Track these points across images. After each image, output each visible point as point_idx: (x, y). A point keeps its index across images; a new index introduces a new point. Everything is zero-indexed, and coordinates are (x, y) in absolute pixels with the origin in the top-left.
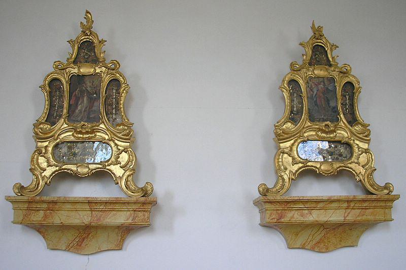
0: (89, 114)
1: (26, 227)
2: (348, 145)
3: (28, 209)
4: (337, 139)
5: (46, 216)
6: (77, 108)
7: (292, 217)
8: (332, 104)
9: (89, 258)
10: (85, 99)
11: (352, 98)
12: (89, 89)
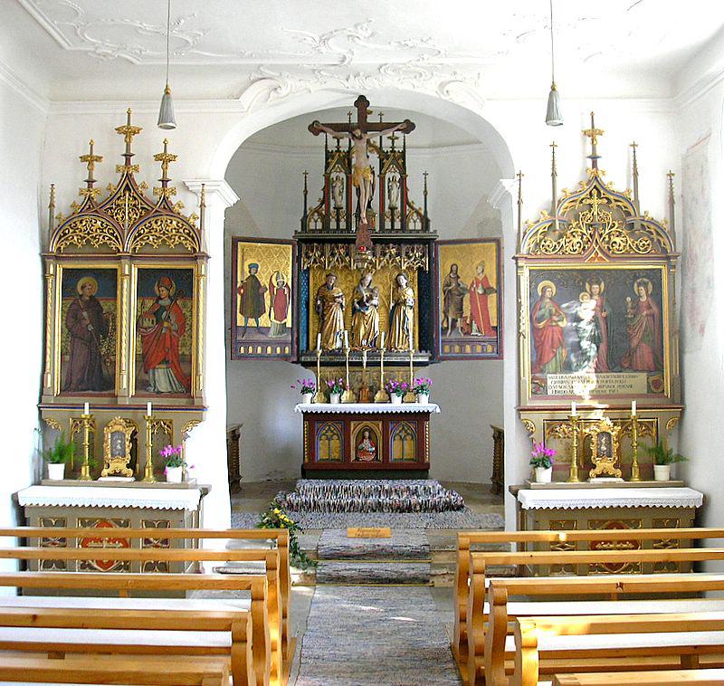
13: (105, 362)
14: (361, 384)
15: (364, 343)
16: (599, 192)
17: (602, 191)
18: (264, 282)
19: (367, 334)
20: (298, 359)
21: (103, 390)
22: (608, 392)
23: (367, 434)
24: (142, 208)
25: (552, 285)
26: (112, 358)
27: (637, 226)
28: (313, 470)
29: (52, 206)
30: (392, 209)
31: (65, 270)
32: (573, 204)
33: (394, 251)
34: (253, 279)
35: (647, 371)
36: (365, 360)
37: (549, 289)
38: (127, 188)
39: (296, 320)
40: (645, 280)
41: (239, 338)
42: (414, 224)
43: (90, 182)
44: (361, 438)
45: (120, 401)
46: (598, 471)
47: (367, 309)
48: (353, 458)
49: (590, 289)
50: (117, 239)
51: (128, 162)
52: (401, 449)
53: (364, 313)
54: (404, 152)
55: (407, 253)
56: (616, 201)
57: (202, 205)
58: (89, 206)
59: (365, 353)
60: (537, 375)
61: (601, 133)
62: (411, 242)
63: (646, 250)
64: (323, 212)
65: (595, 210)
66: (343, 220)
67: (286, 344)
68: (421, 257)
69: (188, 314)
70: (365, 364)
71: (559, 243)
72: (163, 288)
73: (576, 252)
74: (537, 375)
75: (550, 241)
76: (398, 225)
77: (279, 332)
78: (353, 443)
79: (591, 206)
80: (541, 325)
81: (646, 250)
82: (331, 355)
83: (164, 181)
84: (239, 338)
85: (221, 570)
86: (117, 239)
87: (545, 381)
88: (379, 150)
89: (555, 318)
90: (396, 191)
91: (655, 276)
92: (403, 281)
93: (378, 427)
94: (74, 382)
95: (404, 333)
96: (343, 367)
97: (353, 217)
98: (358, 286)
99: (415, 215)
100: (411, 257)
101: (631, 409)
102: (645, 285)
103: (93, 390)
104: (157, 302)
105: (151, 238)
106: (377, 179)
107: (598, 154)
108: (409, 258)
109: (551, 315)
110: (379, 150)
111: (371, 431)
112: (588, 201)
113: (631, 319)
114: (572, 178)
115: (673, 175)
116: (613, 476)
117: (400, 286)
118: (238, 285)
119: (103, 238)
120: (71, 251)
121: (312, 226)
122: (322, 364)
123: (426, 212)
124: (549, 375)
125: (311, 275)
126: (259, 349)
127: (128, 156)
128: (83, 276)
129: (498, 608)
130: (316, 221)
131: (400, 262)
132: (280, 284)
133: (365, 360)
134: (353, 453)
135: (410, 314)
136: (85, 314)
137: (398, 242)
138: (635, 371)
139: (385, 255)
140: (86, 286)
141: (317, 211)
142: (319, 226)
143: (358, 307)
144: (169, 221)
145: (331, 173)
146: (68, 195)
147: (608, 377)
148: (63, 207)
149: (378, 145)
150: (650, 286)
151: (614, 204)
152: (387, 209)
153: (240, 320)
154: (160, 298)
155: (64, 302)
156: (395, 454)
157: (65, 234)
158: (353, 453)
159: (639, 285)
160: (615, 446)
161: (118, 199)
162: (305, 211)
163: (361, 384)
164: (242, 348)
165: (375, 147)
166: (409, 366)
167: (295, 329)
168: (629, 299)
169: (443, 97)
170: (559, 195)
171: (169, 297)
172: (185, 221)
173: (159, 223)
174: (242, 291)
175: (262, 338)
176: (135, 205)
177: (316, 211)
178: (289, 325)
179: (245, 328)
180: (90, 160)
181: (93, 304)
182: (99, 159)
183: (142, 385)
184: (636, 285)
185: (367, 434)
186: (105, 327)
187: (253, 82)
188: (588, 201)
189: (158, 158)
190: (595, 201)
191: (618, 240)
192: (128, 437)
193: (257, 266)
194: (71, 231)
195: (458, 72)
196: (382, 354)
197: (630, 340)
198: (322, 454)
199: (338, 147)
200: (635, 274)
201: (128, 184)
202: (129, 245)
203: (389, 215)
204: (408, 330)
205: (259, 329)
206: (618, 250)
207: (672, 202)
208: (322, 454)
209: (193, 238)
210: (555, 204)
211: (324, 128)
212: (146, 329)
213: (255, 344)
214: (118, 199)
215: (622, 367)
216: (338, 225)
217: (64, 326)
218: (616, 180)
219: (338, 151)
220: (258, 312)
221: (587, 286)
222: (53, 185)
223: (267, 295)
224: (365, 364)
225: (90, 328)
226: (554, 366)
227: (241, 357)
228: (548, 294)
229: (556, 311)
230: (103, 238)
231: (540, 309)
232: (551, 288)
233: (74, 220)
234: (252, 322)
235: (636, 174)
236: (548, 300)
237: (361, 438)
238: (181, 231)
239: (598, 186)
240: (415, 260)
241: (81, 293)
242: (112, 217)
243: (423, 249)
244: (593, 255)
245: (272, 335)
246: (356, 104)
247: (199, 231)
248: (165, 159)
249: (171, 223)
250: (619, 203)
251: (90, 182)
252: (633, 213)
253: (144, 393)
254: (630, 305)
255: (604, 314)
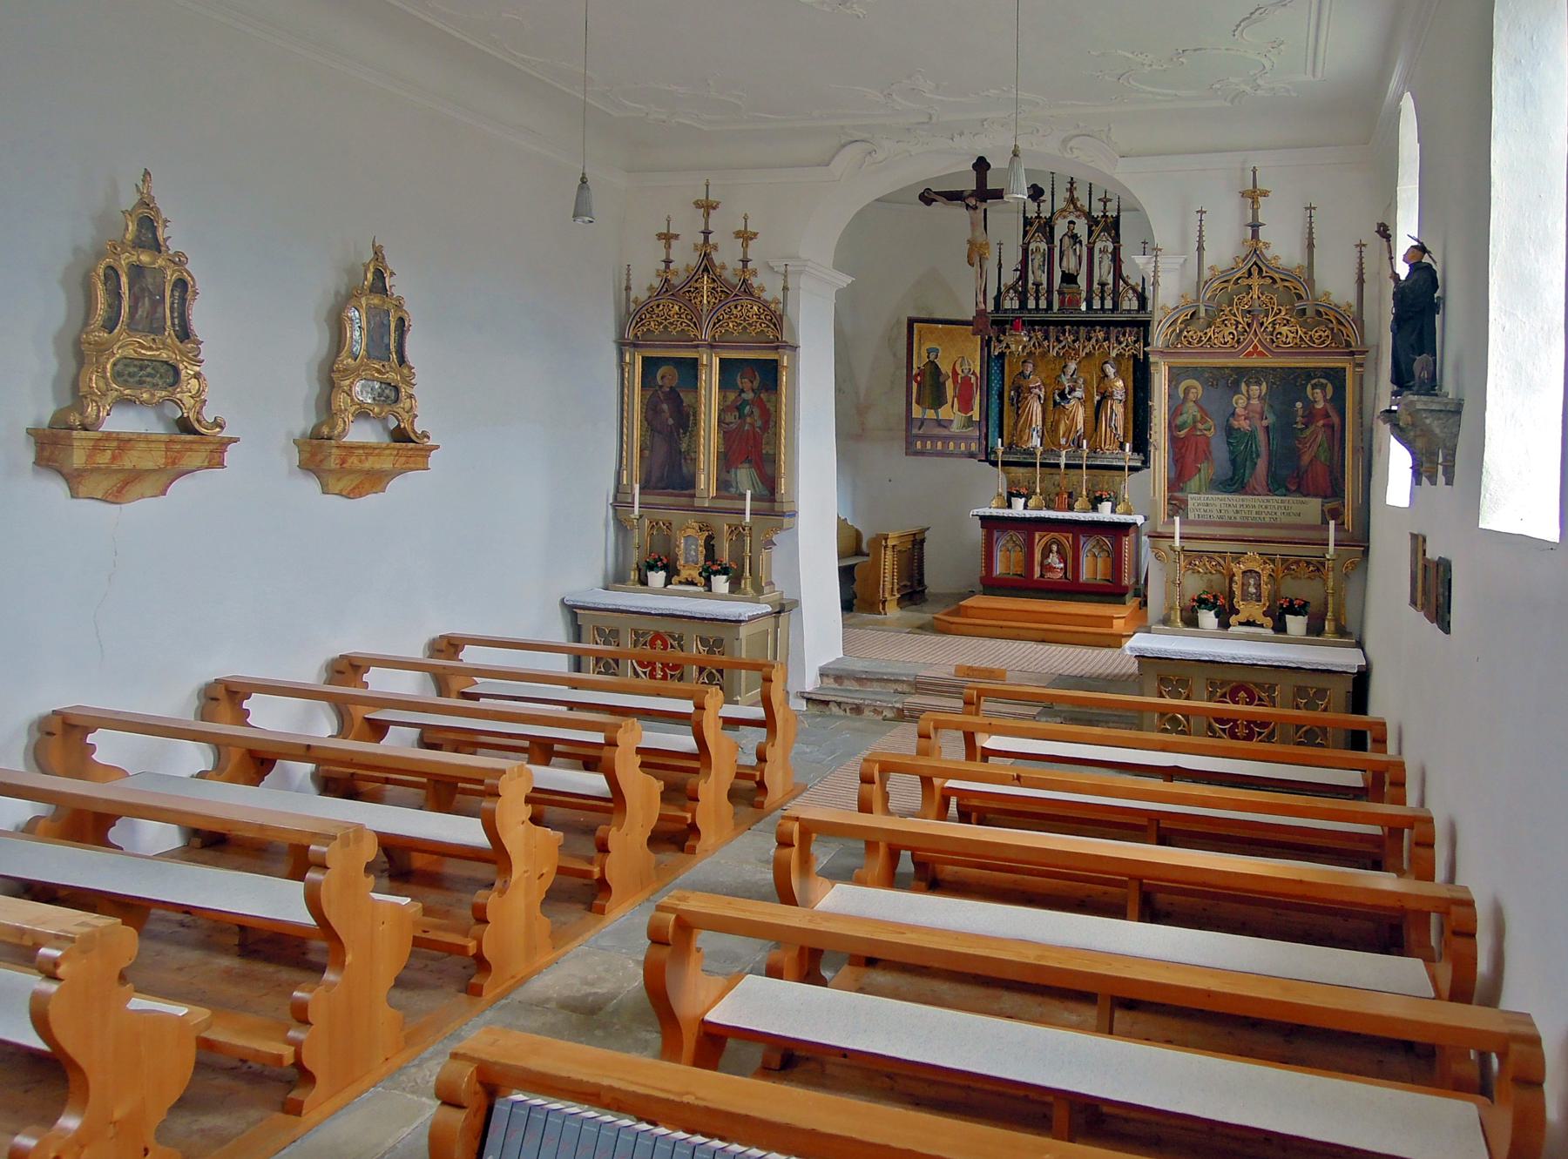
0: (151, 323)
1: (305, 471)
2: (397, 389)
3: (95, 448)
4: (388, 381)
5: (114, 458)
6: (137, 313)
7: (352, 463)
8: (386, 341)
9: (121, 508)
10: (147, 299)
11: (183, 300)
12: (150, 287)
13: (685, 459)
14: (1058, 489)
15: (1063, 441)
16: (1260, 270)
17: (1264, 269)
18: (945, 368)
19: (1068, 431)
20: (987, 457)
21: (683, 489)
22: (1267, 520)
23: (1055, 548)
24: (722, 291)
25: (1200, 387)
26: (692, 454)
27: (1309, 313)
28: (992, 585)
29: (628, 288)
30: (1103, 285)
31: (644, 359)
32: (1225, 285)
33: (1101, 335)
34: (934, 368)
35: (1321, 497)
36: (1063, 461)
37: (1194, 390)
38: (706, 270)
39: (986, 415)
40: (1323, 381)
41: (915, 431)
42: (1130, 303)
43: (668, 262)
44: (1046, 552)
45: (697, 502)
46: (1242, 617)
47: (1068, 402)
48: (1037, 574)
49: (1248, 391)
50: (695, 325)
51: (706, 239)
52: (1091, 567)
53: (1064, 407)
54: (1118, 217)
55: (1117, 337)
56: (1282, 280)
57: (785, 289)
58: (667, 289)
59: (1064, 452)
60: (1176, 494)
61: (1265, 194)
62: (1123, 324)
63: (1323, 342)
64: (1020, 289)
65: (1255, 293)
66: (1043, 297)
67: (972, 439)
68: (1135, 342)
69: (772, 409)
70: (1063, 466)
71: (1206, 333)
72: (746, 380)
73: (1228, 345)
74: (1176, 494)
75: (1193, 332)
76: (1109, 304)
77: (964, 426)
78: (1038, 556)
79: (1250, 287)
80: (1182, 433)
81: (1323, 342)
82: (1028, 454)
83: (745, 262)
84: (915, 431)
85: (806, 695)
86: (695, 325)
87: (1185, 502)
88: (1088, 215)
89: (1200, 426)
90: (1107, 262)
91: (1336, 376)
92: (1110, 370)
93: (1066, 539)
94: (654, 479)
95: (1111, 431)
96: (1080, 471)
97: (1056, 294)
98: (1060, 376)
99: (1131, 291)
100: (1062, 341)
101: (1328, 545)
102: (1323, 387)
103: (673, 489)
104: (740, 395)
105: (731, 325)
106: (1085, 249)
107: (672, 258)
108: (1120, 343)
109: (1195, 422)
110: (1088, 215)
111: (1059, 544)
112: (1246, 282)
113: (1302, 430)
114: (1223, 250)
115: (1364, 245)
116: (1261, 626)
117: (1107, 376)
118: (914, 372)
119: (681, 324)
120: (649, 339)
121: (1007, 305)
122: (1042, 465)
123: (1143, 288)
124: (1190, 495)
125: (1006, 361)
126: (939, 444)
127: (706, 233)
128: (662, 365)
129: (865, 785)
130: (1012, 299)
131: (1109, 347)
132: (966, 371)
133: (1063, 461)
134: (1037, 570)
135: (1119, 409)
136: (665, 407)
137: (1106, 325)
138: (1305, 496)
139: (1089, 339)
140: (666, 377)
141: (1013, 287)
142: (1016, 305)
143: (1057, 401)
144: (671, 305)
145: (1029, 242)
146: (645, 280)
147: (1268, 501)
148: (640, 293)
149: (1087, 209)
150: (1330, 388)
151: (1279, 284)
152: (1096, 286)
153: (917, 412)
154: (742, 391)
155: (644, 393)
156: (1085, 575)
157: (642, 320)
158: (1037, 570)
159: (1314, 387)
160: (1265, 589)
161: (696, 281)
162: (999, 288)
163: (1058, 489)
164: (919, 443)
165: (1083, 212)
166: (1082, 468)
167: (984, 423)
168: (1299, 405)
169: (1067, 156)
170: (1207, 274)
171: (753, 390)
172: (765, 305)
173: (739, 308)
174: (919, 379)
175: (945, 432)
176: (713, 288)
177: (1012, 288)
178: (976, 418)
179: (922, 422)
180: (667, 238)
181: (674, 396)
182: (676, 237)
183: (723, 485)
184: (1309, 388)
185: (1055, 548)
186: (685, 420)
187: (844, 146)
188: (1246, 282)
189: (738, 234)
190: (1255, 281)
191: (1284, 330)
192: (701, 542)
193: (937, 351)
194: (648, 316)
195: (1081, 124)
196: (1085, 456)
197: (1299, 457)
198: (999, 569)
199: (1039, 212)
200: (1309, 374)
201: (707, 265)
202: (706, 335)
203: (1098, 292)
204: (1116, 429)
205: (940, 423)
206: (1285, 343)
207: (1361, 281)
208: (999, 569)
209: (775, 325)
210: (1201, 284)
211: (937, 197)
212: (727, 424)
213: (934, 438)
214: (696, 281)
215: (1288, 490)
216: (1037, 304)
217: (643, 421)
218: (1283, 248)
219: (1038, 217)
220: (938, 400)
221: (1243, 387)
222: (629, 266)
223: (949, 384)
224: (1063, 466)
225: (671, 422)
226: (1198, 483)
227: (917, 453)
228: (1191, 396)
229: (1202, 417)
230: (681, 324)
231: (1181, 414)
232: (1196, 388)
233: (728, 305)
234: (930, 414)
235: (1311, 246)
236: (1192, 404)
237: (1046, 552)
238: (762, 317)
239: (1259, 263)
240: (1127, 346)
241: (660, 383)
242: (690, 300)
243: (1137, 333)
244: (1250, 349)
245: (955, 428)
246: (974, 166)
247: (781, 317)
248: (746, 237)
249: (752, 308)
250: (1286, 284)
251: (668, 262)
252: (1304, 296)
253: (726, 494)
254: (1300, 412)
255: (1265, 423)
